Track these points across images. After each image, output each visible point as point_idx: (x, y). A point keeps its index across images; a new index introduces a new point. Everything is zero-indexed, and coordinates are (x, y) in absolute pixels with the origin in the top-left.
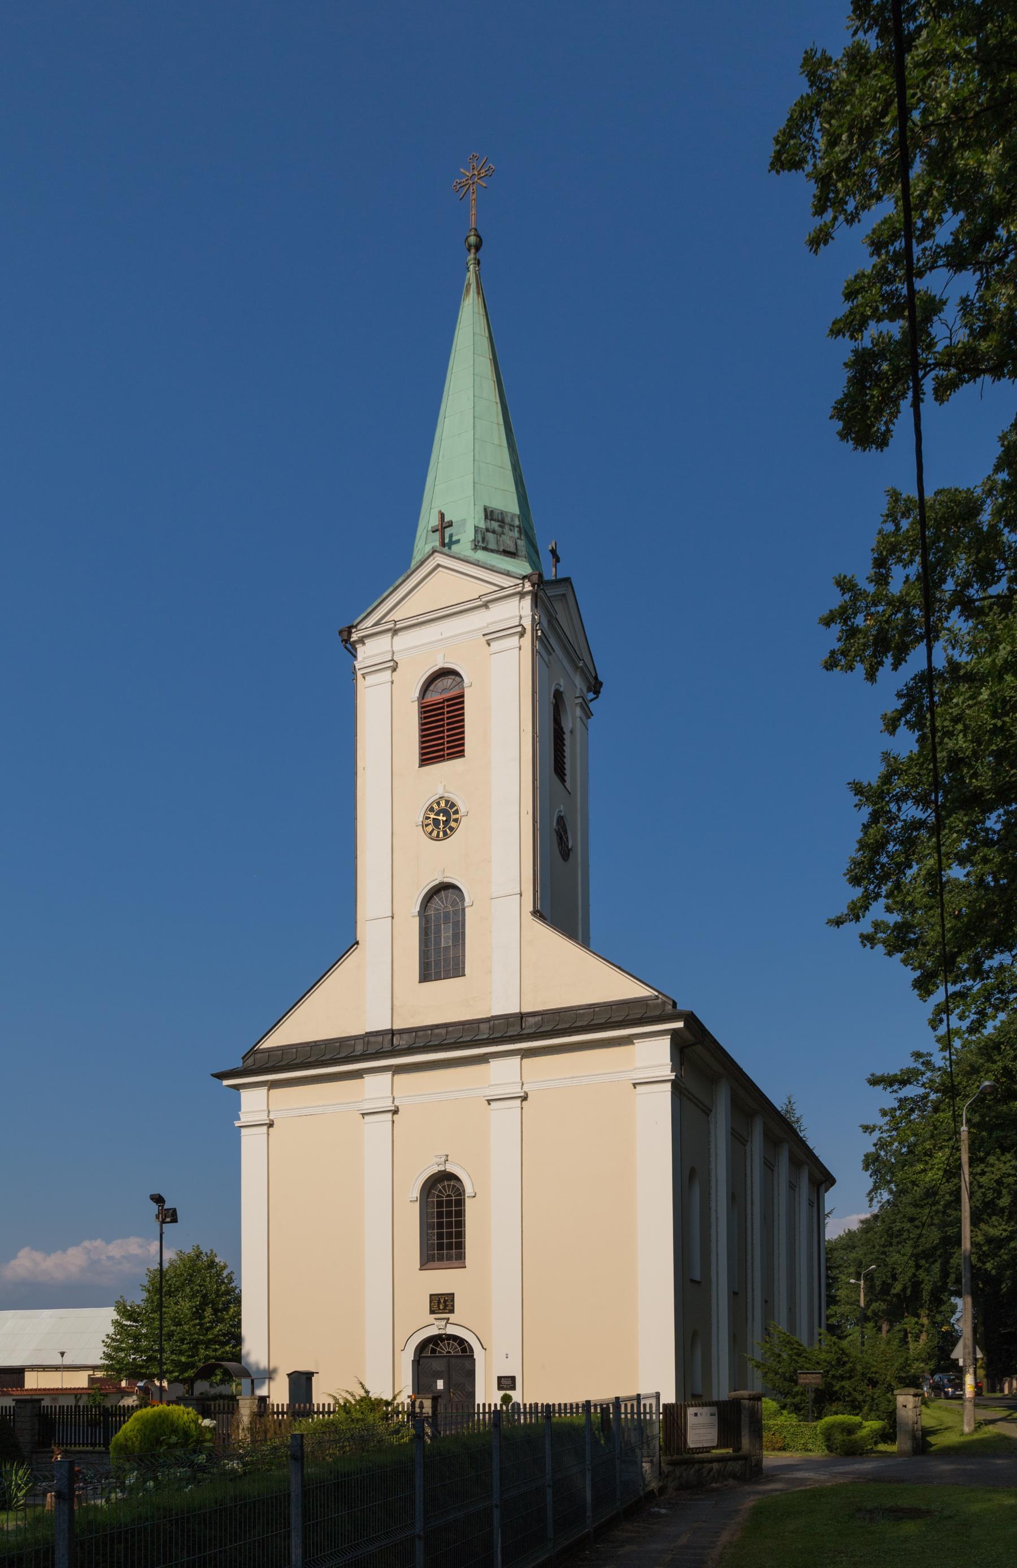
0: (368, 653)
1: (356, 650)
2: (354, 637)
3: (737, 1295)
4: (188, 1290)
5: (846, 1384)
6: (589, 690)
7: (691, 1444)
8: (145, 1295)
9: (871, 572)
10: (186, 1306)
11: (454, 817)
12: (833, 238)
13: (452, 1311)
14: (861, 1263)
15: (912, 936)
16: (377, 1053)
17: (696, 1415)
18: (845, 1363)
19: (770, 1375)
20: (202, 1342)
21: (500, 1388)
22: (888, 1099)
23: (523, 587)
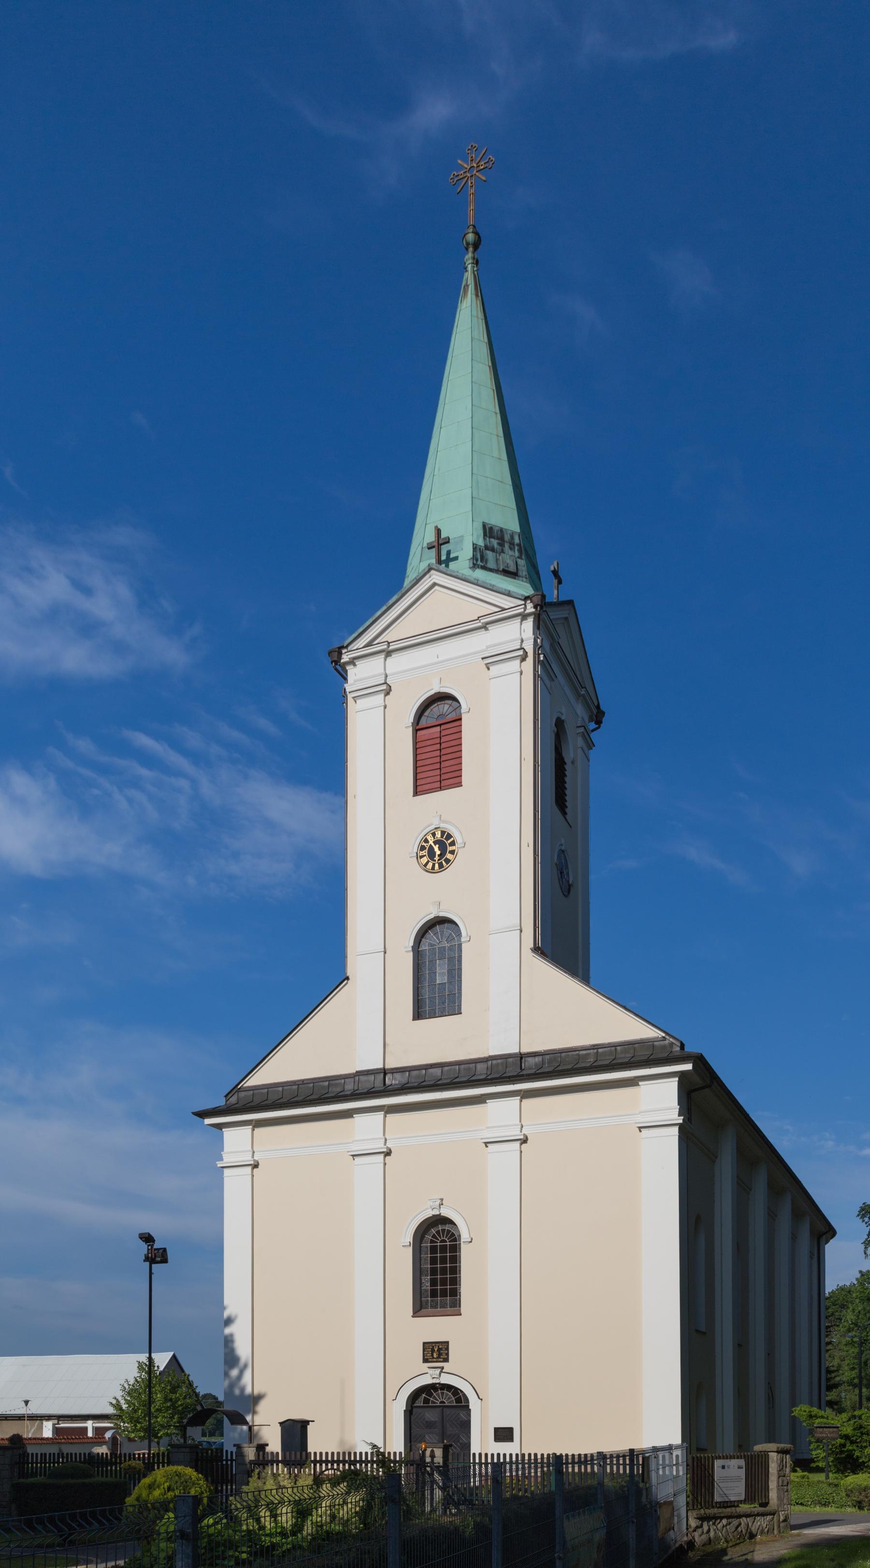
13: (446, 1360)
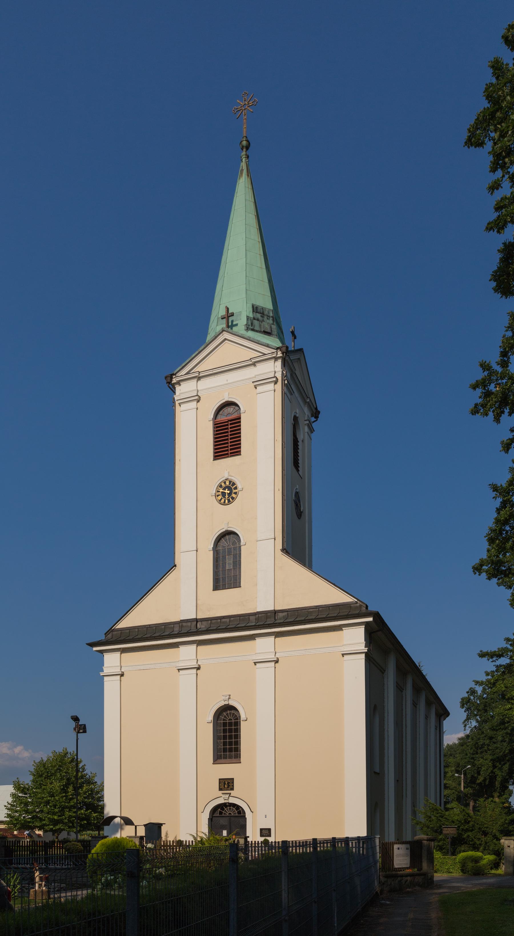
0: (183, 390)
1: (175, 388)
2: (174, 381)
3: (399, 782)
4: (59, 776)
5: (470, 833)
6: (312, 416)
7: (396, 866)
8: (32, 778)
9: (498, 359)
10: (57, 785)
11: (234, 491)
12: (502, 187)
13: (232, 789)
14: (459, 764)
15: (503, 568)
16: (187, 633)
17: (399, 849)
18: (469, 821)
19: (425, 829)
20: (66, 807)
21: (262, 835)
22: (490, 665)
23: (277, 354)
